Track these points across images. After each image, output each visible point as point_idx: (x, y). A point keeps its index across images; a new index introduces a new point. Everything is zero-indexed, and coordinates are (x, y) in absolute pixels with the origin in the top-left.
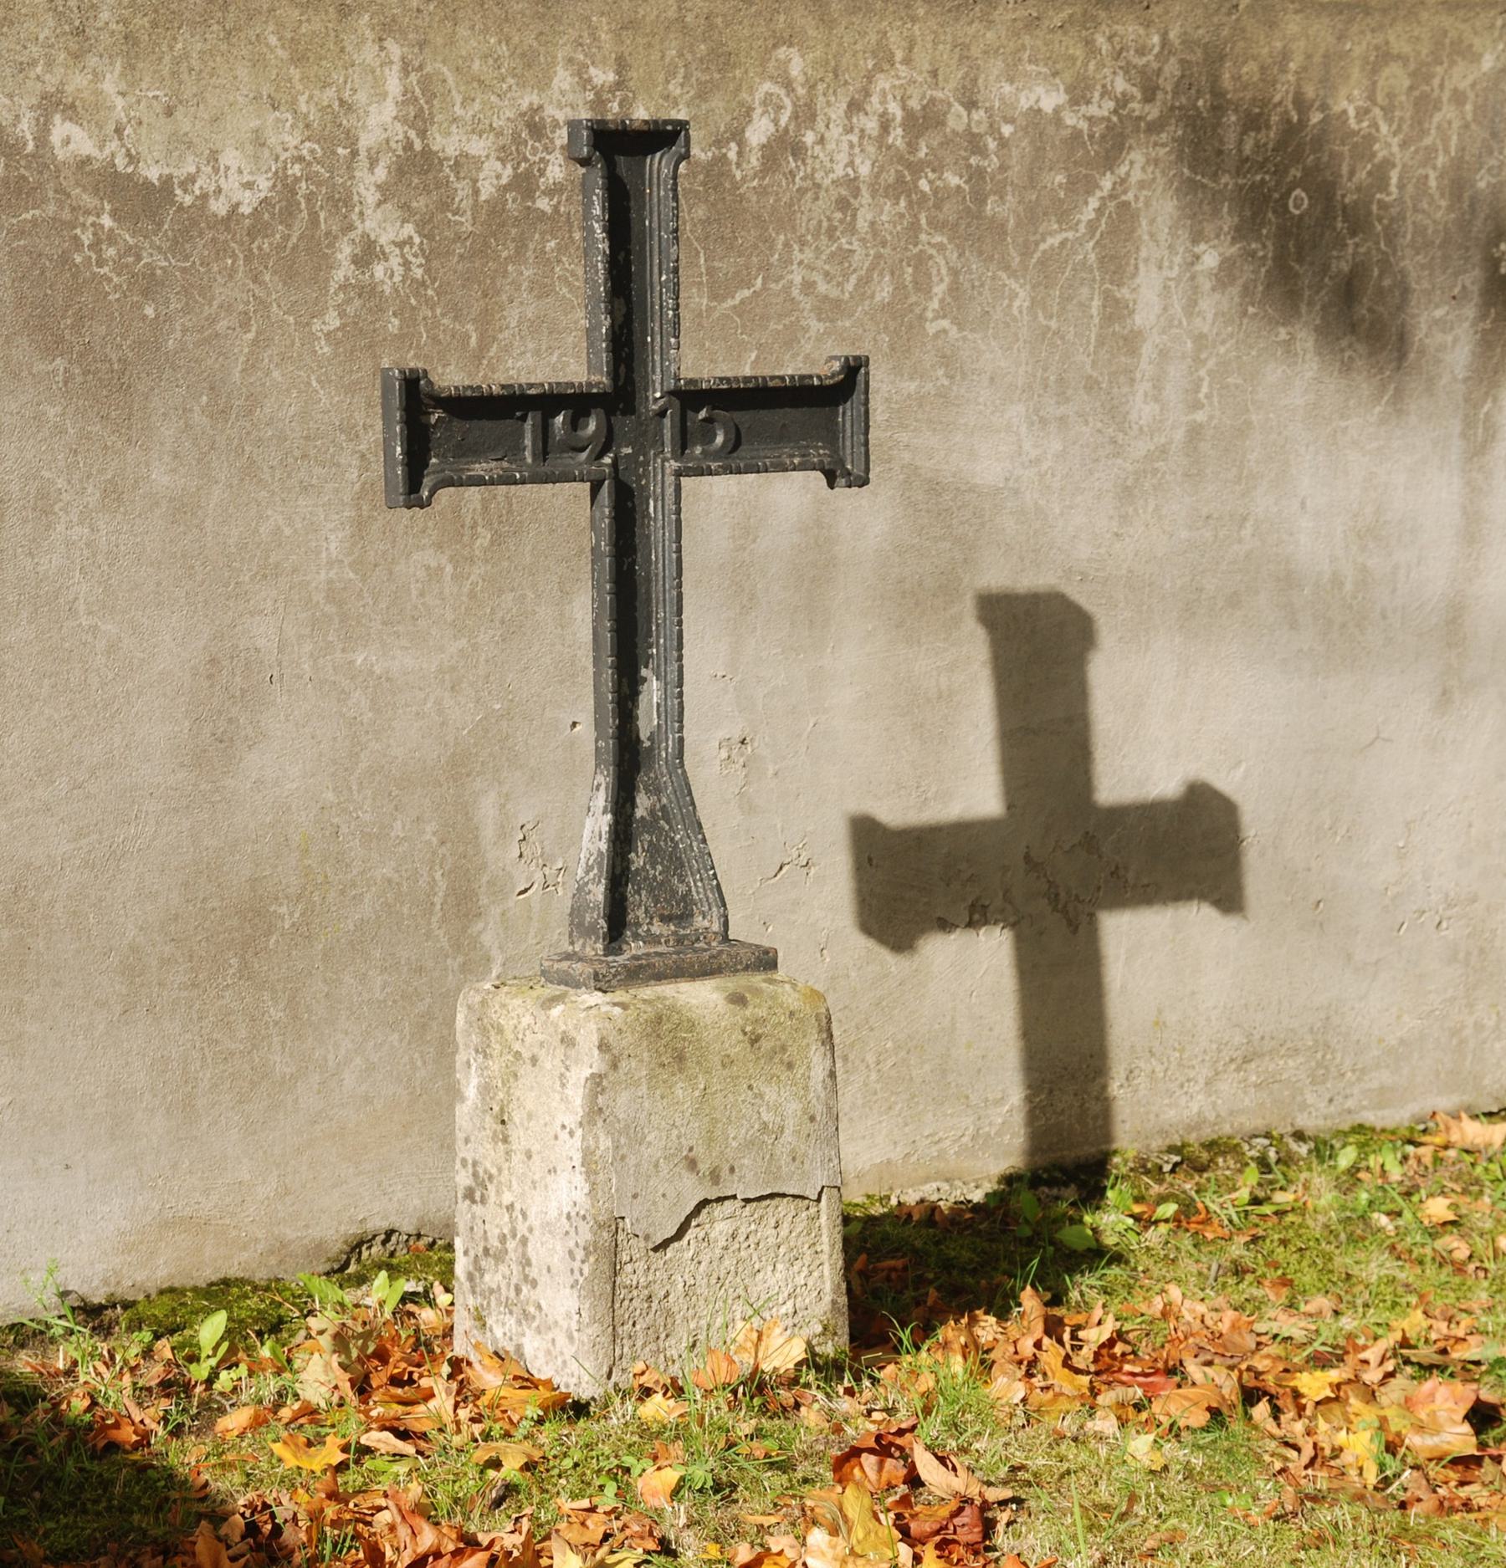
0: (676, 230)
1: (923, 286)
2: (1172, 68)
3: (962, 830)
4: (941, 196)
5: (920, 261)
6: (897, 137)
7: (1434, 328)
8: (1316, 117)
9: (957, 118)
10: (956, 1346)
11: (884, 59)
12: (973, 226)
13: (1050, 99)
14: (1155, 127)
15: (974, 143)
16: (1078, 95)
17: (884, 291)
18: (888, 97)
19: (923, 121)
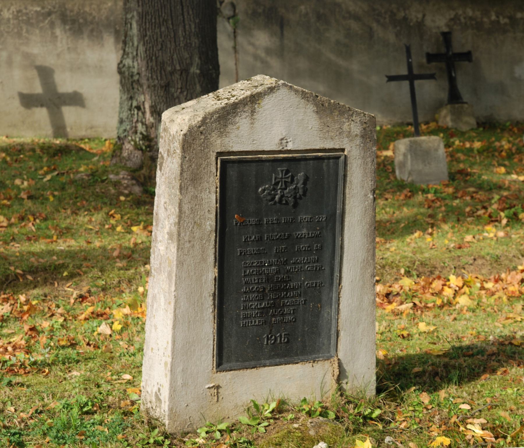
0: (89, 139)
1: (22, 29)
2: (57, 6)
3: (38, 95)
4: (23, 20)
5: (21, 27)
6: (15, 13)
7: (29, 282)
8: (82, 11)
9: (24, 11)
10: (130, 55)
11: (12, 4)
12: (28, 22)
13: (38, 9)
14: (56, 12)
15: (27, 14)
16: (43, 8)
17: (16, 30)
18: (13, 9)
19: (19, 11)
